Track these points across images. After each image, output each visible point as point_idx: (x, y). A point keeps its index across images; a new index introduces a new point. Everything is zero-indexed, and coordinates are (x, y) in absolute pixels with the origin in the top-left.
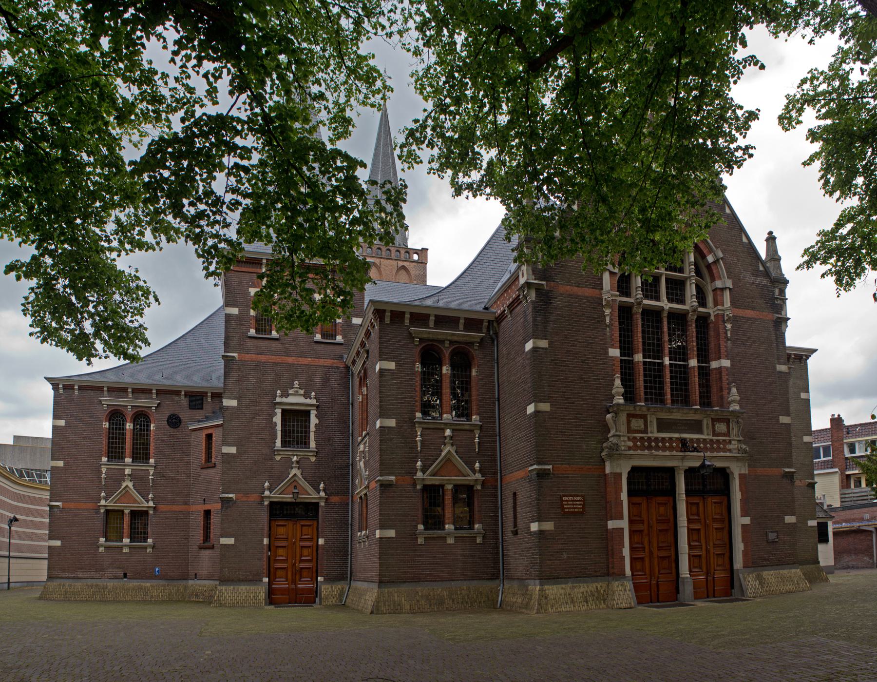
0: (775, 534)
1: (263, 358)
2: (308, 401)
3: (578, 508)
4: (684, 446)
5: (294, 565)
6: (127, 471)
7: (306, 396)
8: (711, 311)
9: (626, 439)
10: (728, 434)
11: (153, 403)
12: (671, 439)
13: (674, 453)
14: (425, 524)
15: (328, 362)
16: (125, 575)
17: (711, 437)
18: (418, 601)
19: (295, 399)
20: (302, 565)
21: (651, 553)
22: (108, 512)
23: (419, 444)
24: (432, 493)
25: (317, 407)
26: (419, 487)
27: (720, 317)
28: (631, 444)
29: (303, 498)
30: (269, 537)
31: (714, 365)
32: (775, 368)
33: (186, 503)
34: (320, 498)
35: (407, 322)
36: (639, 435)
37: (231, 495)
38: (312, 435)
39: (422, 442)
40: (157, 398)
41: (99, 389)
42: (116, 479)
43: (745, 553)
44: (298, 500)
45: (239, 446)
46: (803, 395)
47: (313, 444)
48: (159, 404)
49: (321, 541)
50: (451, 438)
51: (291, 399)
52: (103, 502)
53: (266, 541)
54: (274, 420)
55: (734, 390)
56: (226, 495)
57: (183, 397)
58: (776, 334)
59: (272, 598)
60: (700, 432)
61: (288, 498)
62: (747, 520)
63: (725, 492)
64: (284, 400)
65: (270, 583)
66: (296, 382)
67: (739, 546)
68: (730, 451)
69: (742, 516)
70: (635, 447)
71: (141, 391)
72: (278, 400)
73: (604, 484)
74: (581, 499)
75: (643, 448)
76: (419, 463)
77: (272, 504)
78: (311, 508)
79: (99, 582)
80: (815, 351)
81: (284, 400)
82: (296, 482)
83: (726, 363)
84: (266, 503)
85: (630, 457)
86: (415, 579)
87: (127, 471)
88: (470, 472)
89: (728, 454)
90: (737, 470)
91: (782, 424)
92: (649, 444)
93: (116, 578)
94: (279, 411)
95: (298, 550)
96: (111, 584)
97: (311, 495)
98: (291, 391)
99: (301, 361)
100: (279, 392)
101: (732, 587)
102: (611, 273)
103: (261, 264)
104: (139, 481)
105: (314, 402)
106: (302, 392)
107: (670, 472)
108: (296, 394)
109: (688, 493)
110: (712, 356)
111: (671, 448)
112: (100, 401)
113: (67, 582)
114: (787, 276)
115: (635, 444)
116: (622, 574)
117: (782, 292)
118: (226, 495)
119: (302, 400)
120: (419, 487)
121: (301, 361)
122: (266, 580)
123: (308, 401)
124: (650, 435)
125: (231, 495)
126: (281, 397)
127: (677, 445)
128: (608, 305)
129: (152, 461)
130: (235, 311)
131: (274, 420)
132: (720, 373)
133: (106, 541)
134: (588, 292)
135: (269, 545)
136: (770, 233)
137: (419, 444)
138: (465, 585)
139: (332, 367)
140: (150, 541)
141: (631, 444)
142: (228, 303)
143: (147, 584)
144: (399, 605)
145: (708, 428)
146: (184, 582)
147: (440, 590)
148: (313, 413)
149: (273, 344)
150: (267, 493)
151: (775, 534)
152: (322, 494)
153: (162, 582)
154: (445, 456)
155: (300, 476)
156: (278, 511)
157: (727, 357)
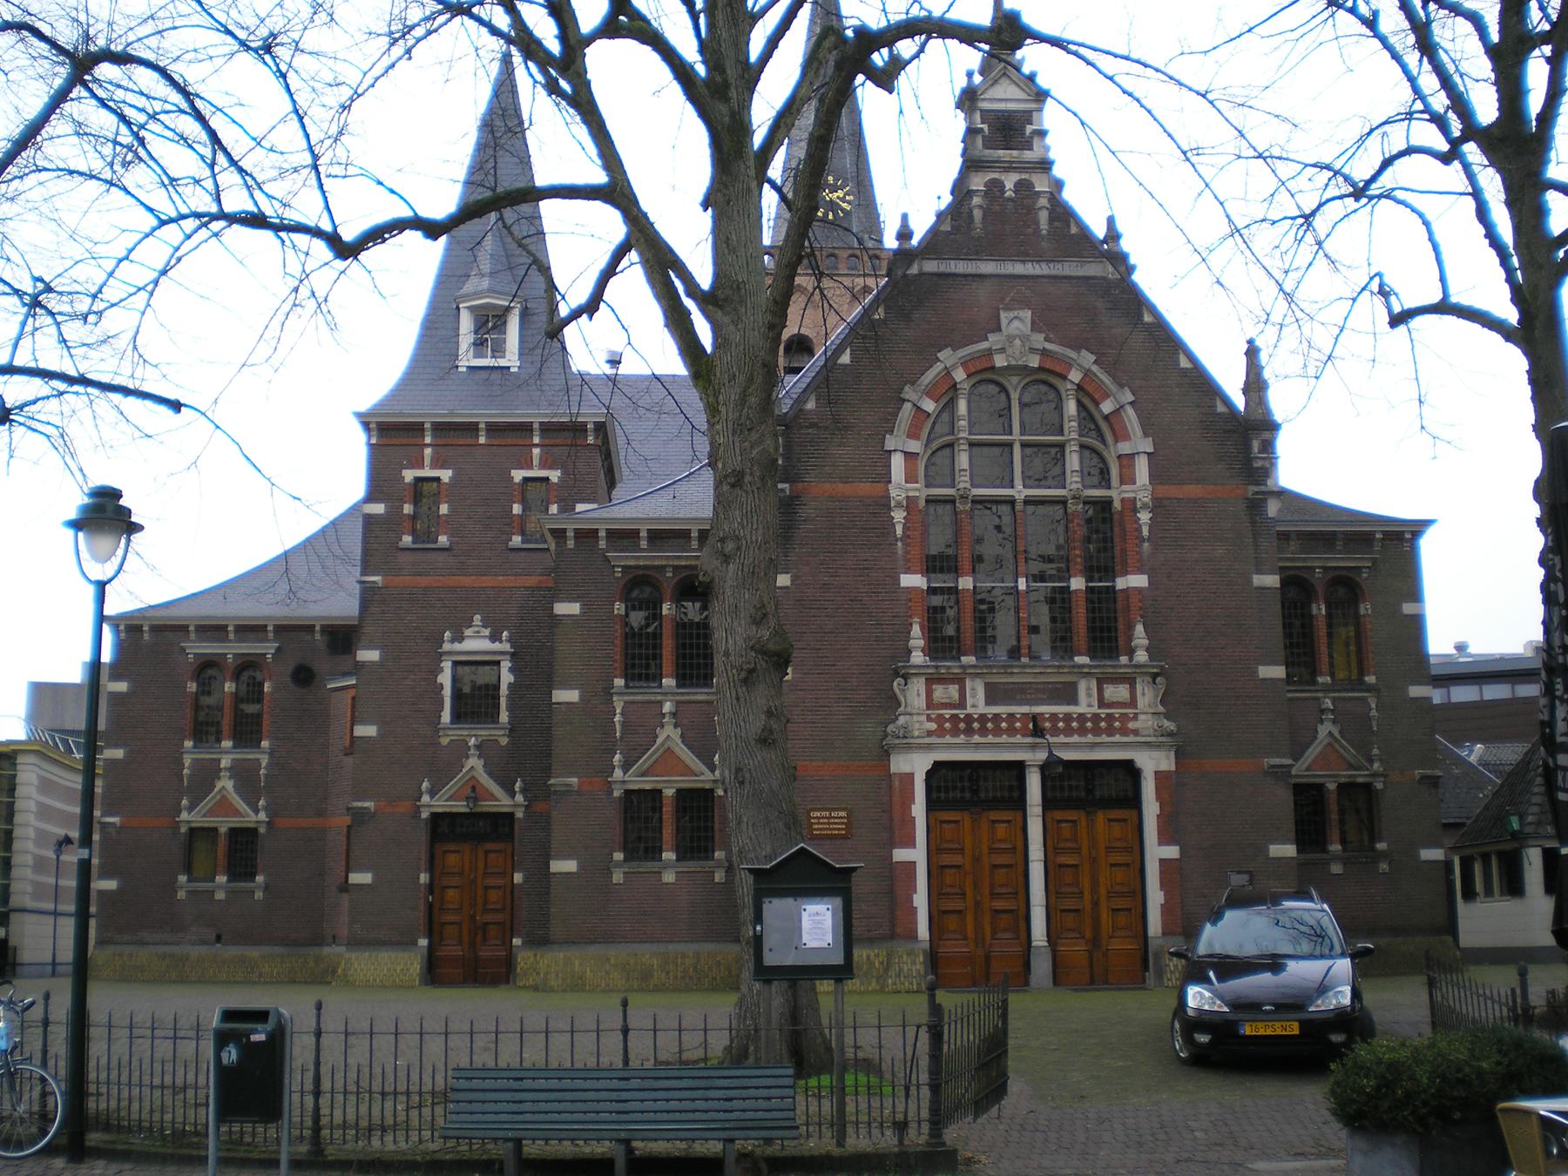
0: (1246, 877)
1: (423, 581)
2: (497, 646)
3: (839, 828)
4: (1037, 728)
5: (473, 917)
6: (225, 762)
7: (494, 637)
8: (1113, 493)
9: (924, 718)
10: (1133, 703)
11: (268, 648)
12: (1011, 715)
13: (1019, 739)
14: (625, 849)
15: (532, 581)
16: (219, 939)
17: (1095, 710)
18: (608, 973)
19: (476, 643)
20: (488, 918)
21: (978, 904)
22: (192, 831)
23: (618, 727)
24: (640, 805)
25: (513, 655)
26: (616, 794)
27: (1131, 506)
28: (933, 726)
29: (487, 806)
30: (431, 869)
31: (1121, 583)
32: (1250, 582)
33: (321, 813)
34: (516, 806)
35: (602, 544)
36: (947, 713)
37: (366, 804)
38: (503, 702)
39: (624, 724)
40: (275, 640)
41: (182, 629)
42: (207, 775)
43: (1166, 909)
44: (479, 810)
45: (382, 724)
46: (1408, 608)
47: (504, 717)
48: (278, 650)
49: (518, 878)
50: (674, 715)
51: (471, 645)
52: (184, 816)
53: (424, 878)
54: (440, 679)
55: (1139, 629)
56: (359, 804)
57: (318, 636)
58: (1253, 523)
59: (435, 973)
60: (1073, 700)
61: (460, 807)
62: (1172, 852)
63: (1133, 801)
64: (457, 647)
65: (430, 946)
66: (477, 617)
67: (1155, 897)
68: (1136, 732)
69: (1160, 844)
70: (940, 732)
71: (250, 630)
72: (447, 647)
73: (895, 790)
74: (843, 814)
75: (955, 732)
76: (617, 757)
77: (436, 817)
78: (501, 824)
79: (175, 950)
80: (1426, 523)
81: (457, 647)
82: (474, 777)
83: (1138, 581)
84: (425, 815)
85: (929, 747)
86: (609, 938)
87: (225, 762)
88: (704, 768)
89: (1131, 738)
90: (1152, 763)
91: (1264, 679)
92: (969, 726)
93: (203, 942)
94: (447, 666)
95: (480, 892)
96: (196, 952)
97: (501, 801)
98: (468, 632)
99: (487, 581)
100: (447, 634)
101: (1146, 967)
102: (909, 456)
103: (423, 430)
104: (245, 777)
105: (506, 647)
106: (487, 632)
107: (1019, 768)
108: (477, 635)
109: (1048, 803)
110: (1118, 568)
111: (1011, 731)
112: (183, 649)
113: (128, 949)
114: (1278, 416)
115: (941, 726)
116: (913, 935)
117: (1268, 447)
118: (359, 804)
119: (485, 645)
120: (616, 794)
121: (487, 581)
122: (423, 942)
123: (497, 646)
124: (969, 710)
125: (366, 804)
126: (452, 641)
127: (1025, 727)
128: (899, 505)
129: (265, 744)
130: (378, 509)
131: (440, 679)
132: (1128, 598)
133: (189, 881)
134: (865, 488)
135: (431, 888)
136: (1250, 342)
137: (618, 727)
138: (690, 948)
139: (539, 588)
140: (260, 879)
141: (933, 726)
142: (370, 498)
143: (254, 952)
144: (580, 978)
145: (1089, 695)
146: (316, 950)
147: (647, 955)
148: (506, 665)
149: (441, 558)
150: (426, 799)
151: (1246, 877)
152: (519, 798)
153: (278, 950)
154: (662, 744)
155: (679, 741)
156: (443, 827)
157: (1140, 571)
